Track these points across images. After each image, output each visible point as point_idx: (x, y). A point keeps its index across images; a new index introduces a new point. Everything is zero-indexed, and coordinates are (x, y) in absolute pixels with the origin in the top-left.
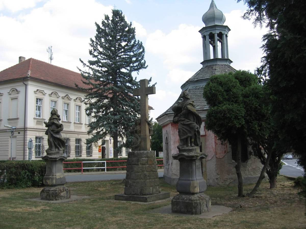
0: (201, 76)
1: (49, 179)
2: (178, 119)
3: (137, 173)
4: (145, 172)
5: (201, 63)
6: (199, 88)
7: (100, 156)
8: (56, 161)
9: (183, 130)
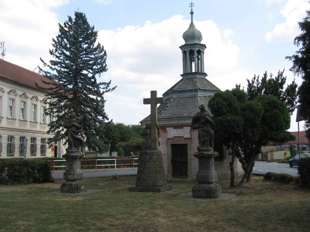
0: (184, 87)
3: (149, 169)
4: (157, 168)
6: (183, 98)
7: (53, 155)
8: (76, 159)
9: (203, 135)
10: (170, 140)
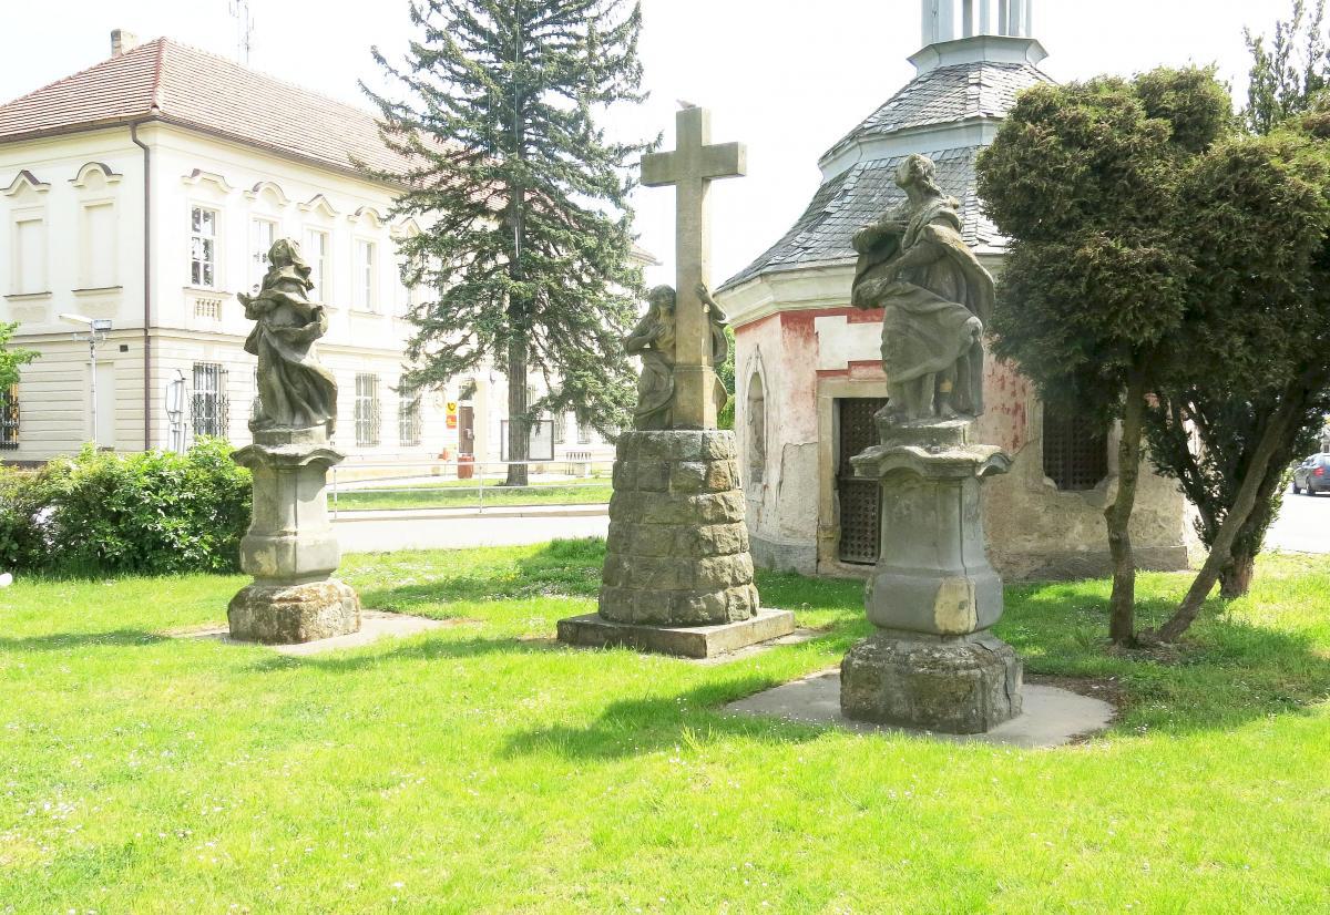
1: (264, 548)
2: (884, 287)
5: (910, 60)
10: (829, 381)
